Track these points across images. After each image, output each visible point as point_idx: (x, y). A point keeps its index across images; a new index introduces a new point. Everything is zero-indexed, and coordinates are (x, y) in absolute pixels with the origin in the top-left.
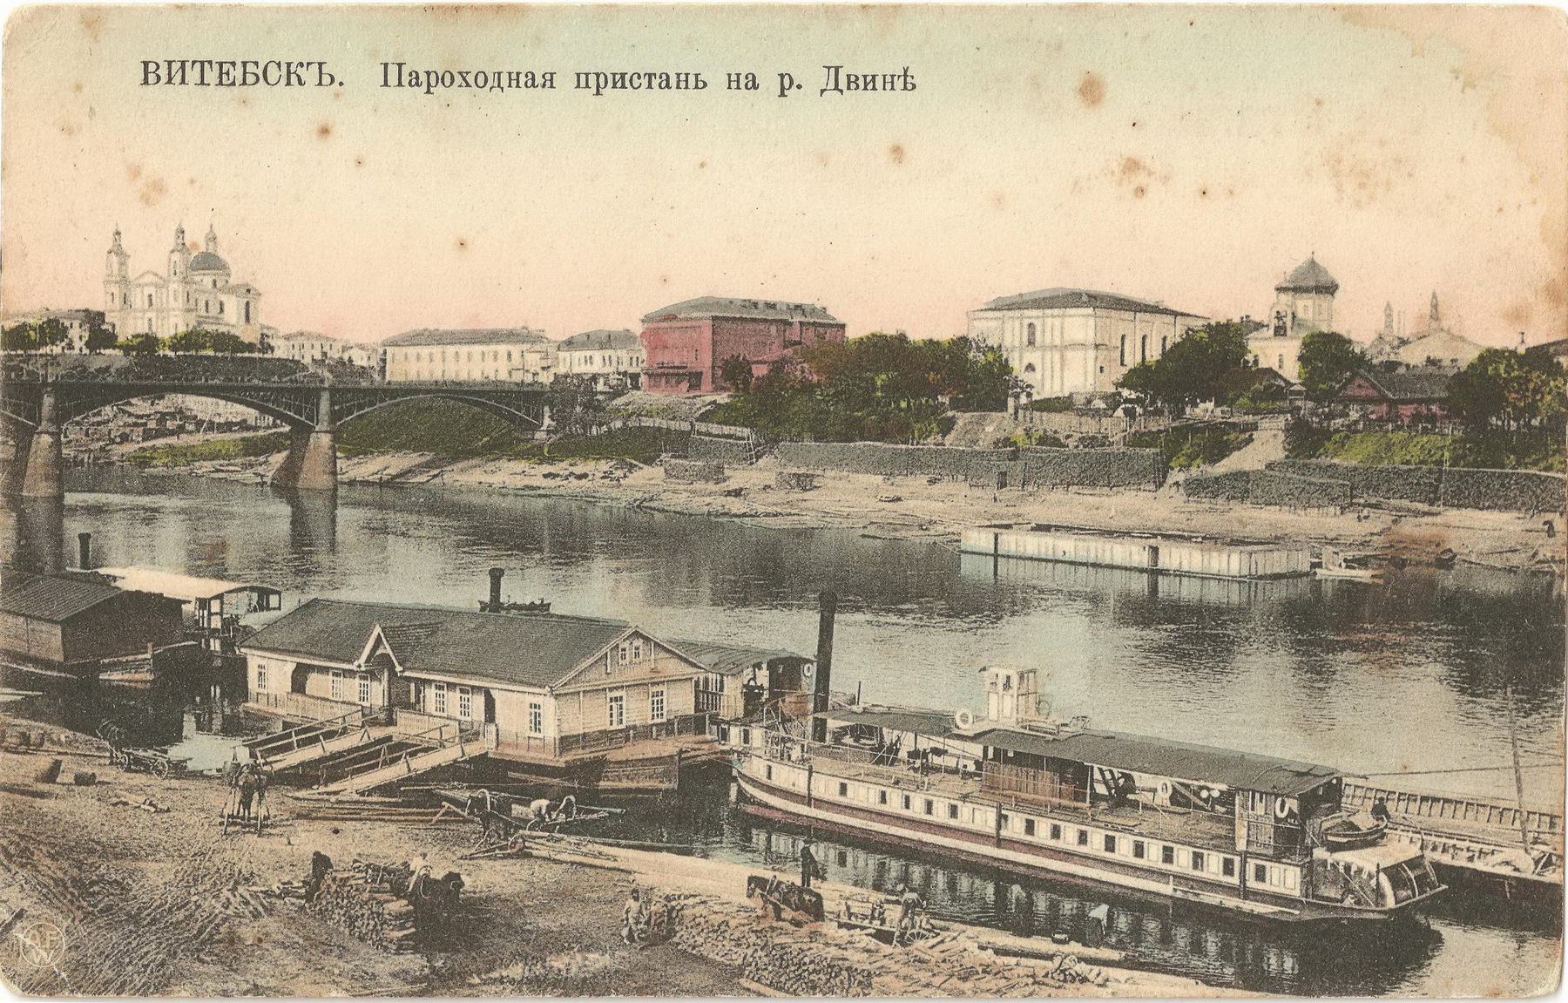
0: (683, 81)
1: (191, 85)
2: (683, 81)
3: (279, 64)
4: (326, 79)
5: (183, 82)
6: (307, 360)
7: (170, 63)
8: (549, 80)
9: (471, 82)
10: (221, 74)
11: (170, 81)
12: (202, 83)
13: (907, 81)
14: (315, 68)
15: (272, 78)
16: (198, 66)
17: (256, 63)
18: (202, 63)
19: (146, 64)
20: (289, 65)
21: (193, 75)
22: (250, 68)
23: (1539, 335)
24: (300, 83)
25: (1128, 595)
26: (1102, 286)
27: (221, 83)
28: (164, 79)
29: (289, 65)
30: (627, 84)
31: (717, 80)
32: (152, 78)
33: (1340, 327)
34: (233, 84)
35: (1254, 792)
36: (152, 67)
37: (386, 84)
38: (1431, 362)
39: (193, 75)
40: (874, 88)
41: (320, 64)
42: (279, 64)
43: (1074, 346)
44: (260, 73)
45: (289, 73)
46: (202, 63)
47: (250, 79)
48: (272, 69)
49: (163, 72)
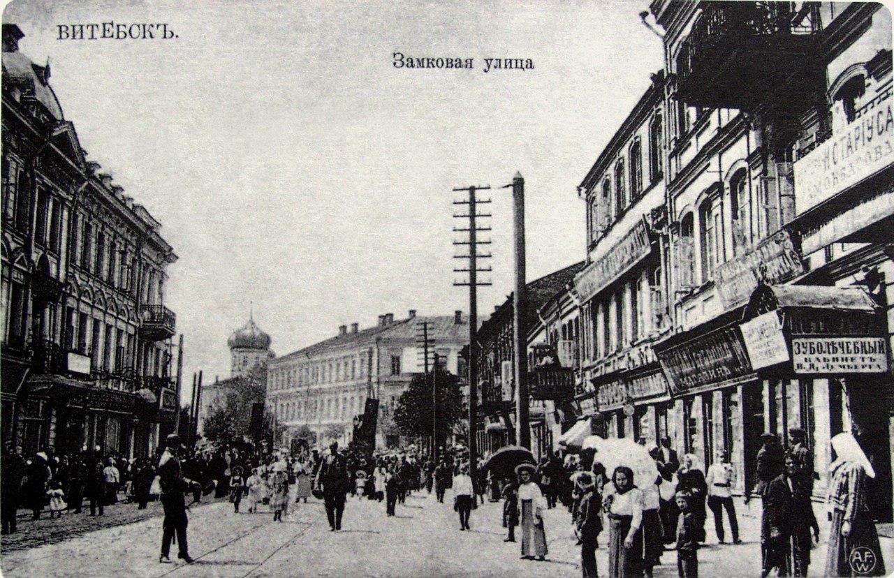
0: (458, 64)
1: (99, 39)
2: (458, 64)
4: (168, 34)
6: (244, 376)
7: (74, 27)
8: (469, 64)
9: (435, 64)
10: (104, 30)
12: (92, 38)
14: (161, 28)
16: (90, 28)
17: (125, 26)
19: (471, 67)
20: (144, 26)
21: (87, 33)
22: (122, 28)
23: (599, 575)
24: (151, 36)
27: (104, 36)
29: (144, 26)
31: (479, 64)
32: (64, 35)
33: (460, 493)
36: (64, 29)
37: (165, 37)
40: (511, 67)
44: (127, 31)
45: (428, 63)
46: (93, 26)
47: (122, 35)
48: (135, 29)
49: (70, 31)
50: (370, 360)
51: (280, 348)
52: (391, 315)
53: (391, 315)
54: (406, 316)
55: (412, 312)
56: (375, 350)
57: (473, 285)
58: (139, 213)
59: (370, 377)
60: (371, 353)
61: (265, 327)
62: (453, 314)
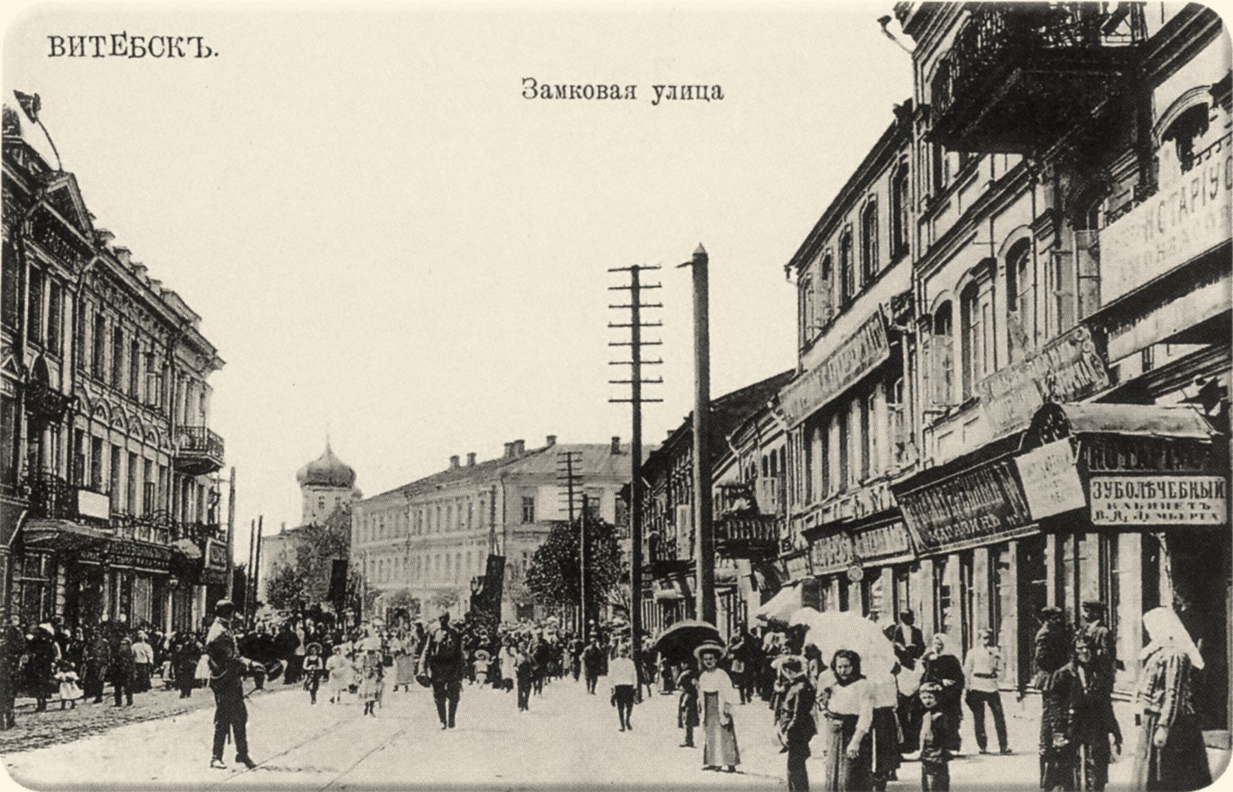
3: (162, 39)
5: (82, 54)
7: (71, 38)
11: (72, 54)
13: (719, 93)
14: (194, 42)
15: (157, 51)
16: (94, 40)
17: (143, 39)
18: (97, 38)
20: (170, 39)
21: (90, 47)
22: (138, 42)
24: (181, 54)
25: (898, 106)
26: (237, 495)
27: (114, 53)
28: (68, 51)
30: (596, 90)
32: (58, 50)
34: (125, 53)
35: (1110, 535)
36: (57, 42)
38: (948, 206)
39: (90, 47)
41: (199, 39)
42: (162, 39)
43: (571, 514)
44: (146, 45)
46: (97, 38)
47: (139, 52)
48: (157, 43)
49: (67, 45)
50: (493, 503)
51: (369, 485)
52: (522, 442)
53: (522, 442)
54: (543, 443)
55: (552, 439)
56: (500, 489)
57: (636, 401)
58: (169, 300)
59: (493, 526)
60: (493, 493)
61: (346, 457)
62: (610, 442)
